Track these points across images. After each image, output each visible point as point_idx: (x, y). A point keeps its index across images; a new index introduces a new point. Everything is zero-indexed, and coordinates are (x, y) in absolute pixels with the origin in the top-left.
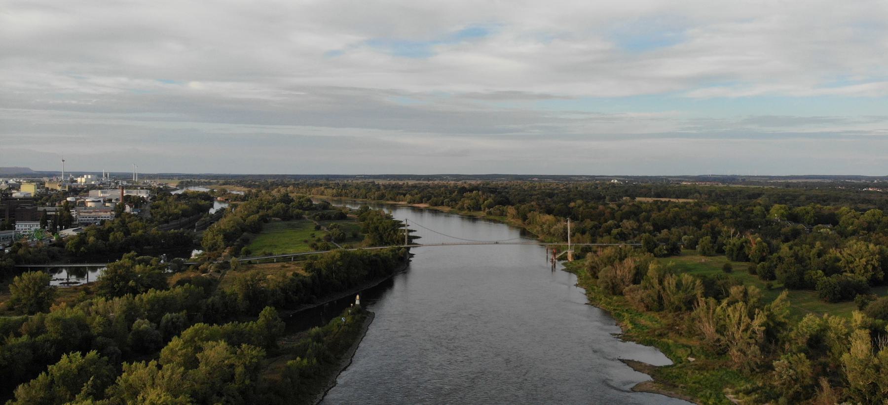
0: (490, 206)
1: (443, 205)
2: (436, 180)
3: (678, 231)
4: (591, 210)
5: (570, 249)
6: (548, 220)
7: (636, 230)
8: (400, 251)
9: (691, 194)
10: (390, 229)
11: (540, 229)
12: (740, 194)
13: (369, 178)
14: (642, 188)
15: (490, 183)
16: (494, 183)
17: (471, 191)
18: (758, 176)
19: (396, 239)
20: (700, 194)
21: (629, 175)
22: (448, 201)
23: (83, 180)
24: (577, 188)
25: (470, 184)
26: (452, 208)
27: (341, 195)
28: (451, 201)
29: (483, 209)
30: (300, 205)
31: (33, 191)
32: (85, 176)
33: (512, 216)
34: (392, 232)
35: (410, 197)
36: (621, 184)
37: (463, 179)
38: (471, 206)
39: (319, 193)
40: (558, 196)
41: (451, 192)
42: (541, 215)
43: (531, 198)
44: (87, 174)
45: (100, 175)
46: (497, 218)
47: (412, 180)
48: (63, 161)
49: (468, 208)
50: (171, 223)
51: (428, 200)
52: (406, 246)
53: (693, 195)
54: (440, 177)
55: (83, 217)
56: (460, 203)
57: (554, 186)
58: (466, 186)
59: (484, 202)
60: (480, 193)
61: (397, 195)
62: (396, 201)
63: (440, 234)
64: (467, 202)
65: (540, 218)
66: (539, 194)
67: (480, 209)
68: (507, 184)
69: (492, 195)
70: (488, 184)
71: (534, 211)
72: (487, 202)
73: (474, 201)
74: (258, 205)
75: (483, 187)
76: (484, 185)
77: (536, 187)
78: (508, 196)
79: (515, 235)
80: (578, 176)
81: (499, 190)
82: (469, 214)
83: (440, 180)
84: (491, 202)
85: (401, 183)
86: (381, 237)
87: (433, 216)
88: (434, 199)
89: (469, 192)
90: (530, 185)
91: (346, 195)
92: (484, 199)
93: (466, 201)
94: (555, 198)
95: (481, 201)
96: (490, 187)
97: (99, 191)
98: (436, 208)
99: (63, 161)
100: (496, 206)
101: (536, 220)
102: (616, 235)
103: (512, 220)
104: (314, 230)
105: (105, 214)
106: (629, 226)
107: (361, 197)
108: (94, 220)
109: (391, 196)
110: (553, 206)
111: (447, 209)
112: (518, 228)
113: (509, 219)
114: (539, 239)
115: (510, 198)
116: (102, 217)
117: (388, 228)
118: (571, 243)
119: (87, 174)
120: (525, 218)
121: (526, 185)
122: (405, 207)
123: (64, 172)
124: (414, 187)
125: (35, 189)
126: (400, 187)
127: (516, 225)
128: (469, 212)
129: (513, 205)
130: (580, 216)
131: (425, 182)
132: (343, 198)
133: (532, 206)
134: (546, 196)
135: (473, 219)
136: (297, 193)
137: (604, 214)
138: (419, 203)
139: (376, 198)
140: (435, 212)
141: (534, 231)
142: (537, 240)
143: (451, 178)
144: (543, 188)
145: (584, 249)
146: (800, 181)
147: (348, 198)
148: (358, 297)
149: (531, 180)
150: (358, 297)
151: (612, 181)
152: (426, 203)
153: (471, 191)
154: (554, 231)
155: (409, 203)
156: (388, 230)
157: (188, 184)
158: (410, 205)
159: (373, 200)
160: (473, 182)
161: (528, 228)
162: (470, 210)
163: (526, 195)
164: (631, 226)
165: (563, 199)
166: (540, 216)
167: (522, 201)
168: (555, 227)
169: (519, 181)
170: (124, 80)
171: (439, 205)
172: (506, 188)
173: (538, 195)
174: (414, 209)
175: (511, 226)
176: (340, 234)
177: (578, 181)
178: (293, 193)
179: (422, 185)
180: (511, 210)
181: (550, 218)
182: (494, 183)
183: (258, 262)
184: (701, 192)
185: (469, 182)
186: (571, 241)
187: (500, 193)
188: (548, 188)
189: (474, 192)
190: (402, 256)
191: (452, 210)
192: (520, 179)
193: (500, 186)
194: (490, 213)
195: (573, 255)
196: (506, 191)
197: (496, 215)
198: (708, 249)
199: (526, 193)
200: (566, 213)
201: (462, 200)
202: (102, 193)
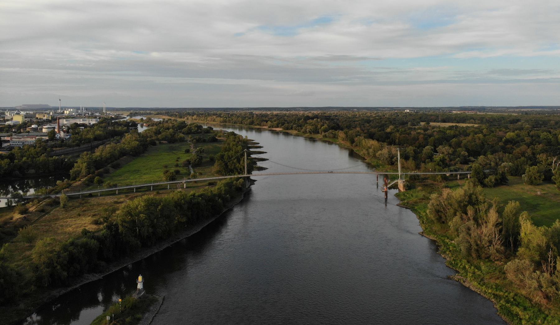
0: (325, 131)
1: (293, 130)
2: (292, 111)
3: (495, 158)
4: (407, 135)
5: (401, 178)
6: (373, 145)
7: (451, 155)
8: (238, 182)
9: (468, 120)
10: (234, 157)
11: (366, 152)
12: (504, 119)
13: (251, 110)
14: (432, 116)
15: (326, 112)
16: (329, 112)
17: (313, 118)
18: (498, 107)
19: (238, 166)
20: (475, 120)
21: (415, 106)
22: (296, 126)
23: (68, 112)
24: (384, 116)
25: (313, 114)
26: (298, 131)
27: (226, 122)
28: (298, 126)
29: (320, 133)
30: (189, 130)
31: (21, 120)
32: (69, 110)
34: (235, 160)
35: (270, 123)
36: (412, 113)
37: (309, 110)
38: (311, 130)
39: (212, 120)
40: (373, 122)
41: (299, 120)
42: (366, 139)
43: (354, 124)
44: (71, 108)
45: (78, 109)
46: (331, 140)
47: (278, 111)
48: (60, 100)
49: (310, 132)
50: (82, 146)
51: (282, 125)
52: (245, 175)
53: (470, 120)
54: (295, 109)
55: (14, 142)
56: (304, 128)
57: (369, 114)
58: (310, 115)
59: (321, 127)
60: (319, 120)
61: (262, 122)
62: (261, 126)
63: (278, 164)
64: (309, 128)
65: (365, 143)
66: (360, 120)
67: (318, 133)
68: (337, 113)
69: (327, 122)
70: (325, 113)
71: (360, 136)
72: (323, 128)
73: (314, 127)
74: (155, 131)
75: (321, 116)
76: (322, 114)
77: (357, 115)
78: (338, 122)
79: (345, 154)
80: (382, 108)
81: (332, 118)
82: (310, 136)
83: (295, 111)
84: (326, 128)
85: (269, 113)
86: (226, 165)
88: (286, 125)
89: (311, 120)
90: (353, 114)
91: (229, 121)
92: (321, 125)
93: (308, 127)
94: (371, 123)
95: (319, 126)
96: (326, 115)
97: (64, 120)
99: (60, 100)
100: (330, 131)
101: (362, 143)
102: (438, 162)
103: (342, 142)
104: (184, 152)
105: (31, 139)
106: (445, 151)
107: (238, 123)
108: (22, 144)
109: (258, 122)
110: (373, 130)
111: (294, 132)
112: (346, 149)
113: (340, 141)
114: (366, 161)
115: (340, 124)
116: (28, 142)
117: (232, 157)
118: (402, 171)
119: (71, 108)
120: (352, 142)
121: (350, 114)
122: (266, 130)
123: (61, 107)
124: (277, 115)
125: (22, 118)
126: (266, 116)
127: (346, 147)
128: (310, 135)
129: (342, 129)
130: (397, 141)
131: (284, 112)
132: (227, 124)
133: (358, 132)
134: (365, 122)
135: (313, 140)
136: (199, 120)
137: (418, 139)
138: (276, 127)
139: (248, 124)
140: (287, 134)
141: (361, 153)
142: (363, 162)
143: (302, 110)
144: (361, 116)
145: (413, 177)
146: (546, 110)
147: (230, 124)
148: (140, 278)
149: (352, 111)
150: (140, 278)
151: (406, 111)
152: (281, 127)
153: (313, 118)
154: (379, 155)
155: (270, 127)
156: (233, 158)
157: (136, 114)
158: (270, 129)
159: (246, 125)
160: (315, 112)
161: (355, 150)
162: (311, 134)
163: (351, 121)
164: (446, 151)
165: (377, 124)
166: (365, 141)
167: (349, 127)
168: (380, 152)
169: (345, 111)
170: (113, 51)
171: (289, 129)
172: (337, 116)
173: (359, 122)
175: (341, 147)
176: (196, 159)
177: (383, 111)
178: (196, 120)
179: (282, 114)
180: (341, 134)
181: (373, 143)
182: (329, 112)
183: (99, 195)
184: (475, 118)
185: (313, 112)
186: (403, 167)
187: (333, 120)
188: (365, 116)
189: (315, 119)
190: (240, 186)
191: (298, 133)
192: (345, 110)
193: (333, 114)
194: (325, 136)
195: (404, 186)
196: (336, 119)
197: (330, 137)
198: (535, 178)
199: (351, 120)
200: (387, 139)
201: (305, 125)
202: (66, 121)
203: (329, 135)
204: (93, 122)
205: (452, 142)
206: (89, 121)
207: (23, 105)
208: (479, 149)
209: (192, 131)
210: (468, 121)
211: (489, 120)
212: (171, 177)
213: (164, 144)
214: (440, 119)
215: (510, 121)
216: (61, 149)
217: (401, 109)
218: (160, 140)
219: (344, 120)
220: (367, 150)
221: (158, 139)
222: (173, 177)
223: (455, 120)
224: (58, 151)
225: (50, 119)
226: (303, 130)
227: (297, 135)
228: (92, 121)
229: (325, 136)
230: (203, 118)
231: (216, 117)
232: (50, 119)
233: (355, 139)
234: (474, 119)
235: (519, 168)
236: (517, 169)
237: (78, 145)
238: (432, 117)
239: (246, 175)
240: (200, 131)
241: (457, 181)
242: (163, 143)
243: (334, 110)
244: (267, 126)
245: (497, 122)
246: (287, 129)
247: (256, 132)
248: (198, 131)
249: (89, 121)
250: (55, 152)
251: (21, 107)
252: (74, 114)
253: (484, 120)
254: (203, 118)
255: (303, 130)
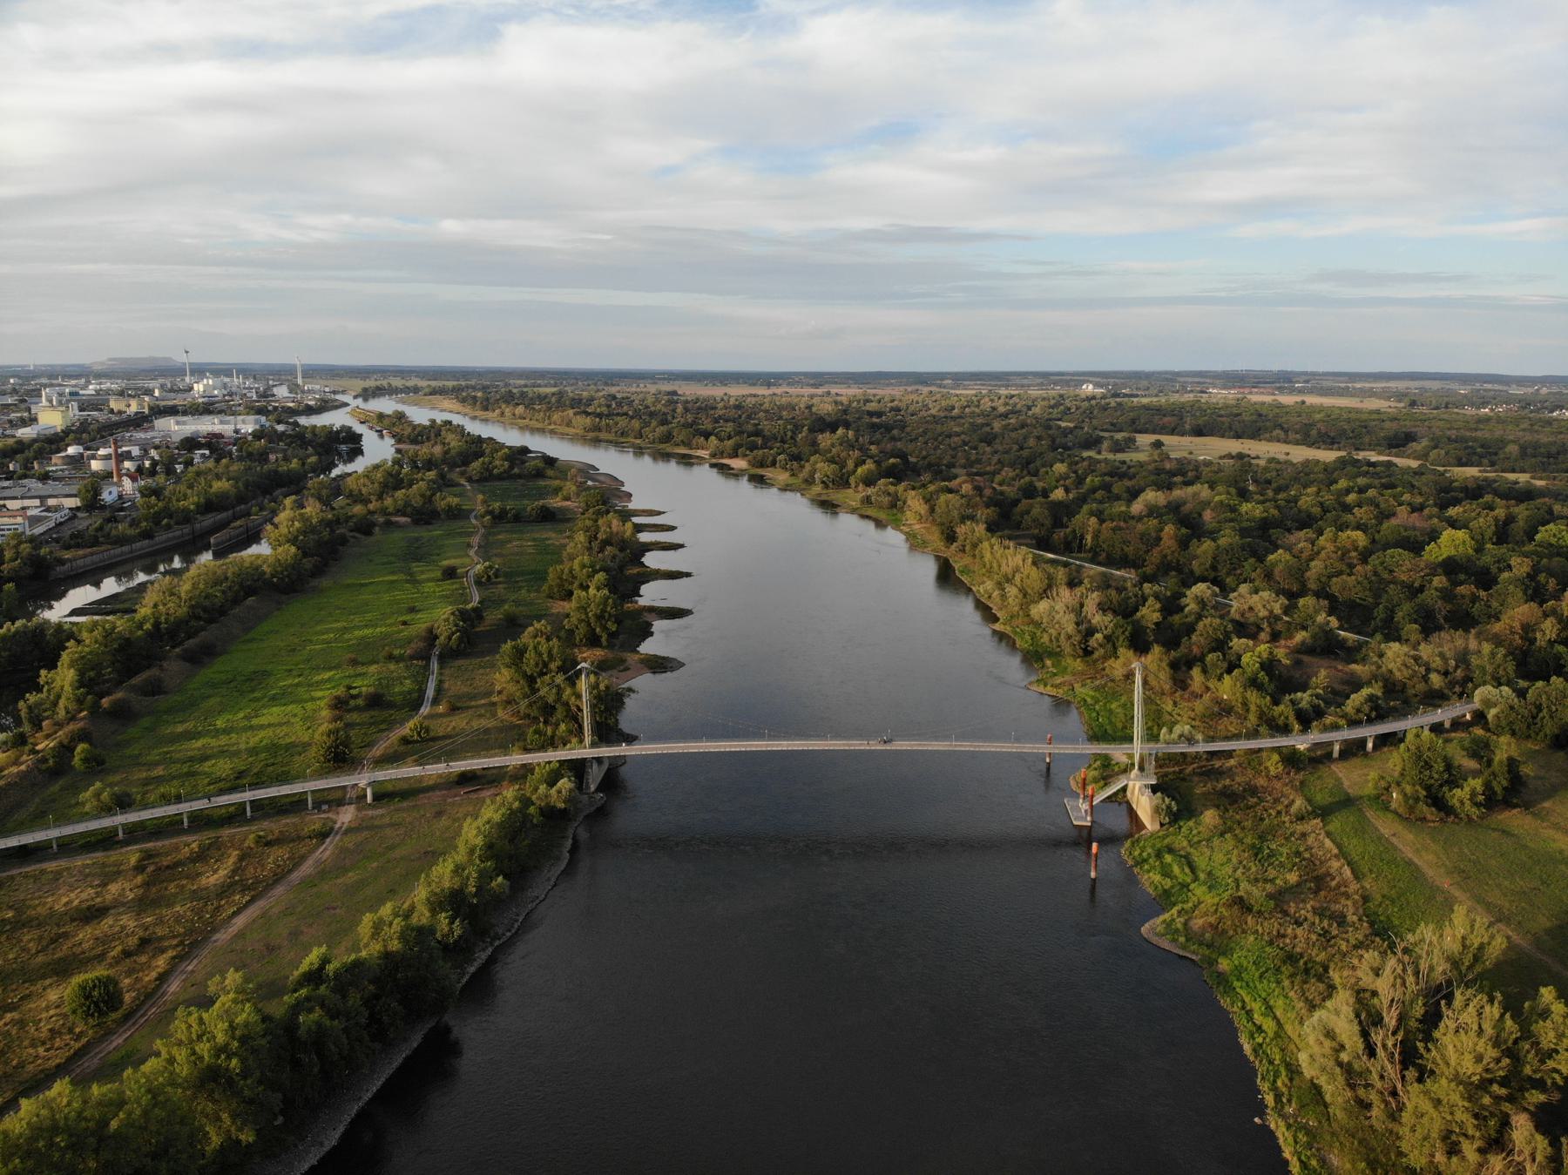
9: (1266, 429)
20: (1286, 431)
26: (793, 475)
27: (600, 430)
29: (853, 485)
33: (918, 517)
37: (516, 933)
46: (882, 516)
48: (187, 352)
49: (823, 482)
56: (808, 467)
67: (847, 485)
82: (824, 498)
87: (756, 487)
95: (850, 464)
98: (760, 471)
99: (187, 352)
111: (783, 477)
120: (950, 538)
130: (1089, 538)
132: (603, 435)
134: (981, 441)
138: (731, 457)
140: (759, 480)
158: (714, 461)
164: (1264, 606)
170: (346, 218)
173: (963, 436)
174: (724, 470)
176: (453, 634)
178: (525, 418)
193: (889, 405)
203: (879, 499)
204: (248, 426)
205: (1274, 564)
206: (235, 425)
207: (110, 360)
208: (1370, 600)
209: (495, 471)
210: (1268, 435)
211: (1326, 433)
212: (329, 748)
213: (400, 527)
214: (1187, 427)
215: (1385, 438)
216: (92, 554)
217: (1069, 378)
218: (390, 514)
219: (921, 430)
220: (1000, 585)
221: (384, 512)
222: (337, 747)
223: (1230, 428)
224: (80, 562)
225: (146, 411)
226: (805, 474)
227: (785, 488)
228: (244, 422)
229: (867, 500)
230: (542, 414)
231: (575, 414)
232: (146, 411)
233: (958, 530)
234: (1282, 428)
235: (1541, 715)
236: (1534, 718)
237: (147, 535)
238: (1166, 419)
239: (593, 745)
240: (516, 470)
241: (1333, 767)
242: (397, 522)
243: (892, 384)
244: (707, 449)
245: (1350, 441)
246: (762, 465)
247: (678, 463)
248: (513, 472)
249: (235, 425)
250: (68, 566)
251: (102, 363)
252: (216, 392)
253: (1314, 432)
254: (542, 414)
255: (805, 474)
